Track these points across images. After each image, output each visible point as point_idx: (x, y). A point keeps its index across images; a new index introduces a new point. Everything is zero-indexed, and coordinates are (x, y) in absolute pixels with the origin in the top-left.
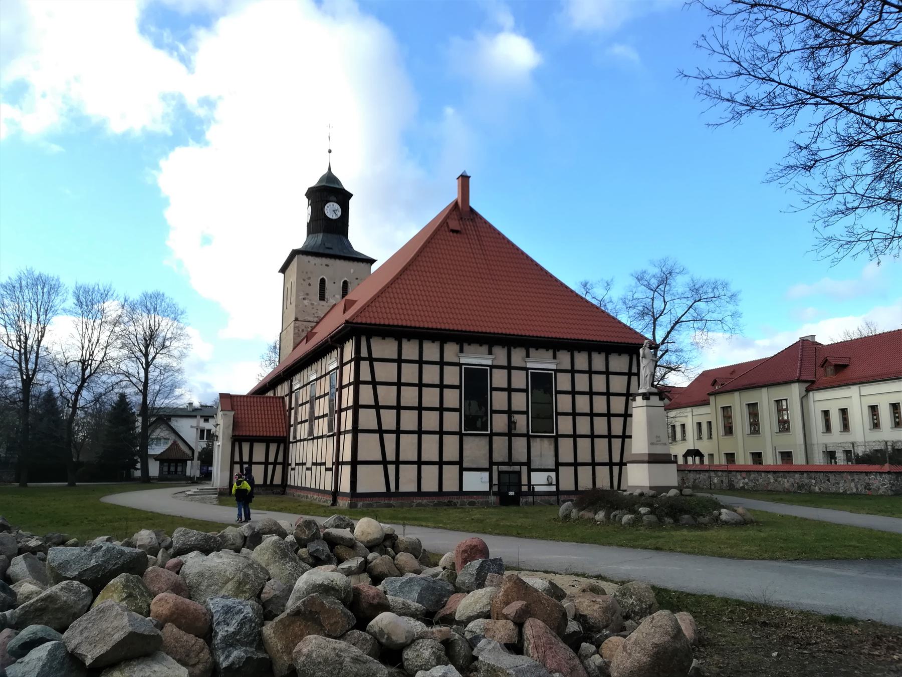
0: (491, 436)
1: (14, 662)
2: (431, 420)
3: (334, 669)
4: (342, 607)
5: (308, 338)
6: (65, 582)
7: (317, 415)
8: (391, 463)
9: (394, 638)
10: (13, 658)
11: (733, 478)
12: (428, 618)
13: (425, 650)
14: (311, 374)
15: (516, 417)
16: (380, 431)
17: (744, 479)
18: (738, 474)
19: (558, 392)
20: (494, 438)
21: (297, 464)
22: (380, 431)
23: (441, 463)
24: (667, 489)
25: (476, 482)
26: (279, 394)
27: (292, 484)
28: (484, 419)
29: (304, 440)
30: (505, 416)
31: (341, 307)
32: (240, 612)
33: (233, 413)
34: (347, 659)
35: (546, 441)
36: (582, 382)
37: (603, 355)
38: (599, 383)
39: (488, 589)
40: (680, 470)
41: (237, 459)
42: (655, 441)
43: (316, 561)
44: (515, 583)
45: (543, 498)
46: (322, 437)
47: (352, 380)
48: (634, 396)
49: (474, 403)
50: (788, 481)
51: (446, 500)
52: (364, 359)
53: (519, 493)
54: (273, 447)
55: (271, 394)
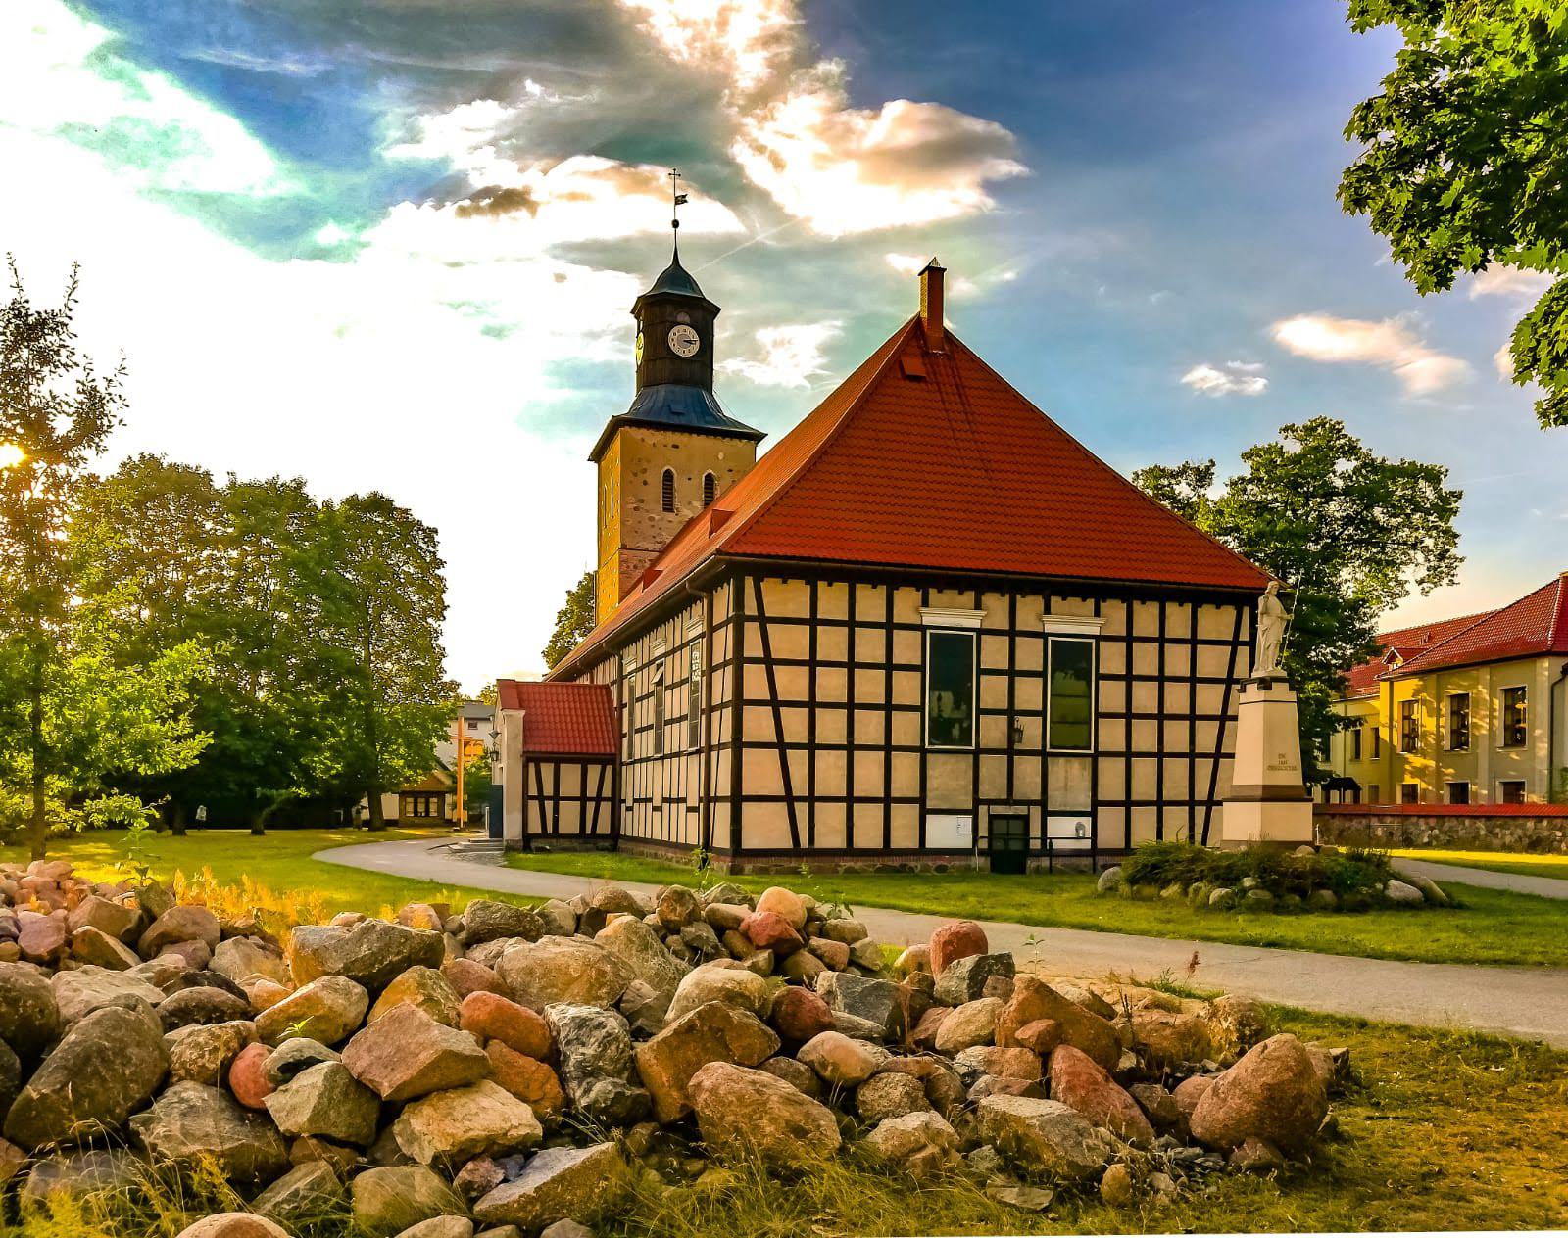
0: (977, 753)
1: (275, 1090)
2: (869, 728)
3: (754, 1111)
4: (757, 1022)
5: (650, 576)
6: (326, 978)
7: (668, 717)
8: (549, 798)
9: (843, 1069)
10: (271, 1085)
11: (1412, 828)
12: (891, 1041)
13: (895, 1087)
14: (655, 645)
15: (1022, 722)
16: (782, 746)
17: (1432, 829)
18: (1422, 821)
19: (1100, 677)
20: (982, 757)
21: (635, 801)
22: (782, 746)
23: (887, 800)
24: (1295, 845)
25: (949, 832)
26: (599, 681)
27: (629, 834)
28: (965, 725)
29: (648, 759)
30: (1004, 719)
31: (706, 523)
32: (600, 1026)
33: (523, 713)
34: (775, 1098)
35: (1076, 764)
36: (1146, 659)
37: (882, 590)
38: (1178, 660)
39: (988, 1000)
40: (1318, 813)
41: (533, 791)
42: (1276, 762)
43: (698, 954)
44: (1037, 991)
45: (1067, 861)
46: (678, 755)
47: (730, 656)
48: (1243, 685)
49: (947, 697)
50: (1512, 834)
51: (896, 862)
52: (751, 619)
53: (1027, 852)
54: (594, 771)
55: (585, 680)
